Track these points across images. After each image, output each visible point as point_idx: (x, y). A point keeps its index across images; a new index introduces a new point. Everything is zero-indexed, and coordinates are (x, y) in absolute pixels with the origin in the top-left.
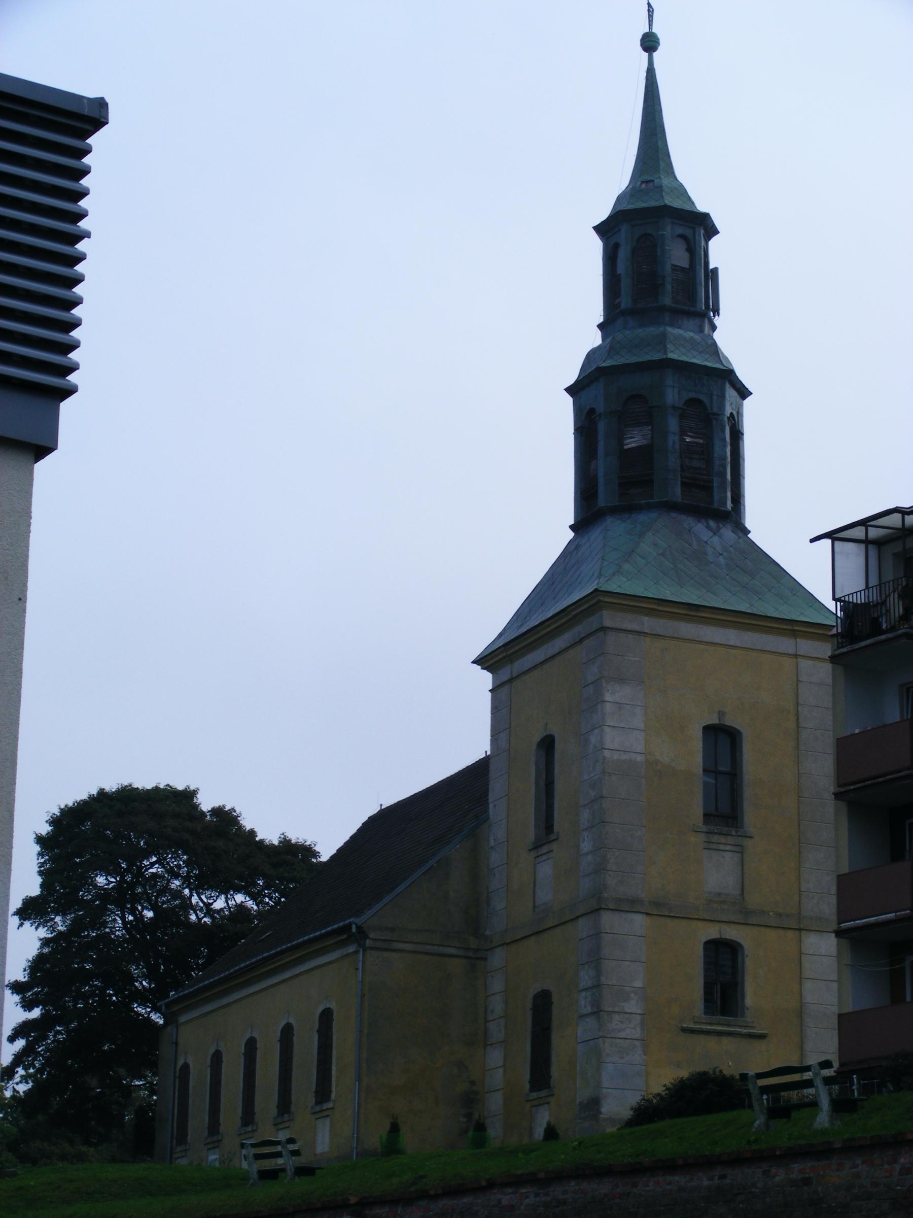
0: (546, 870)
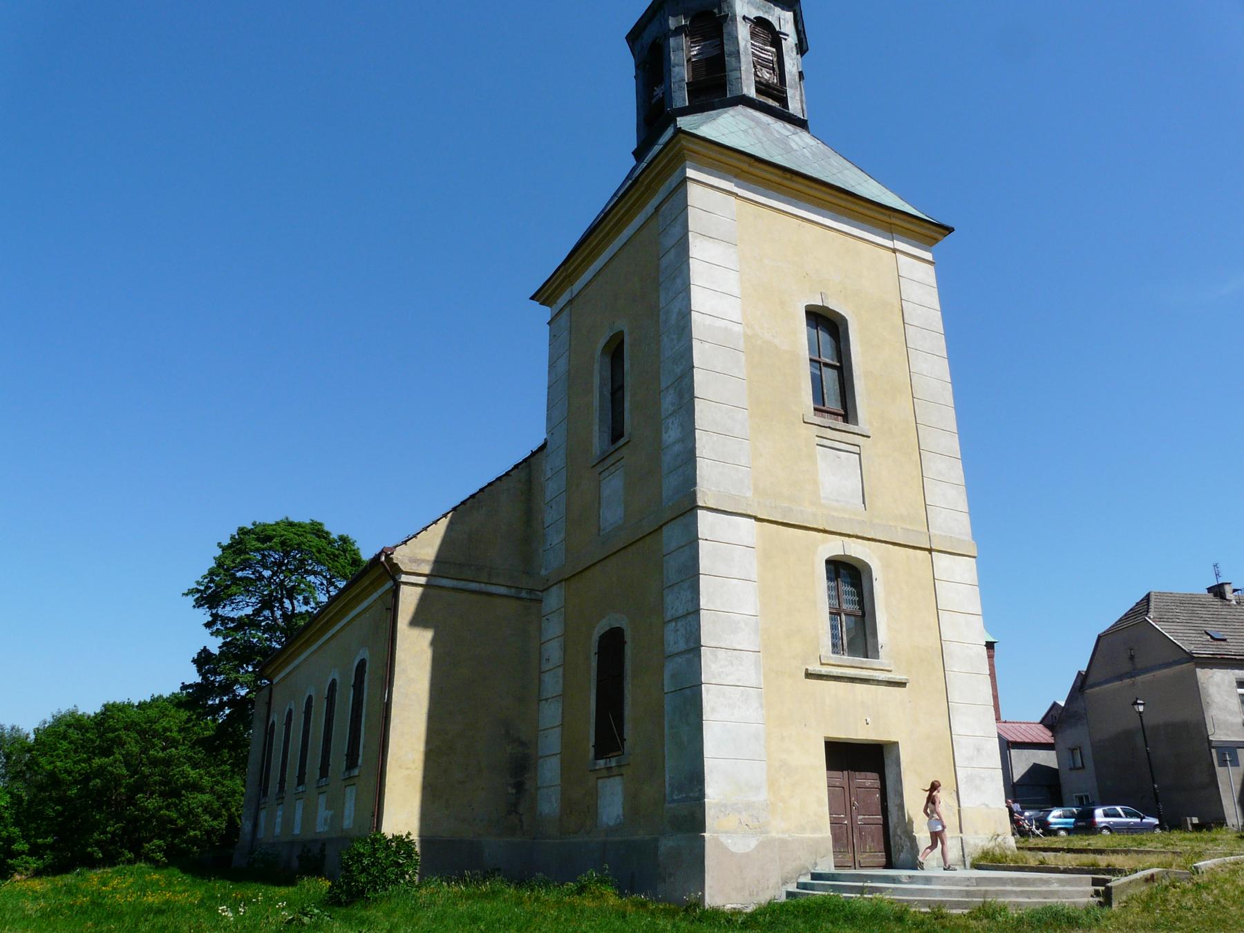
0: (613, 485)
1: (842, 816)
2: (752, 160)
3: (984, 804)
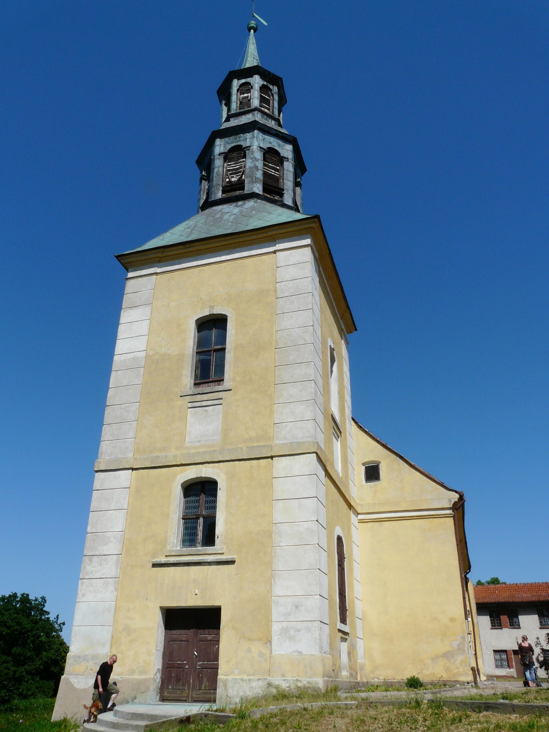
1: (185, 662)
2: (162, 250)
3: (297, 651)
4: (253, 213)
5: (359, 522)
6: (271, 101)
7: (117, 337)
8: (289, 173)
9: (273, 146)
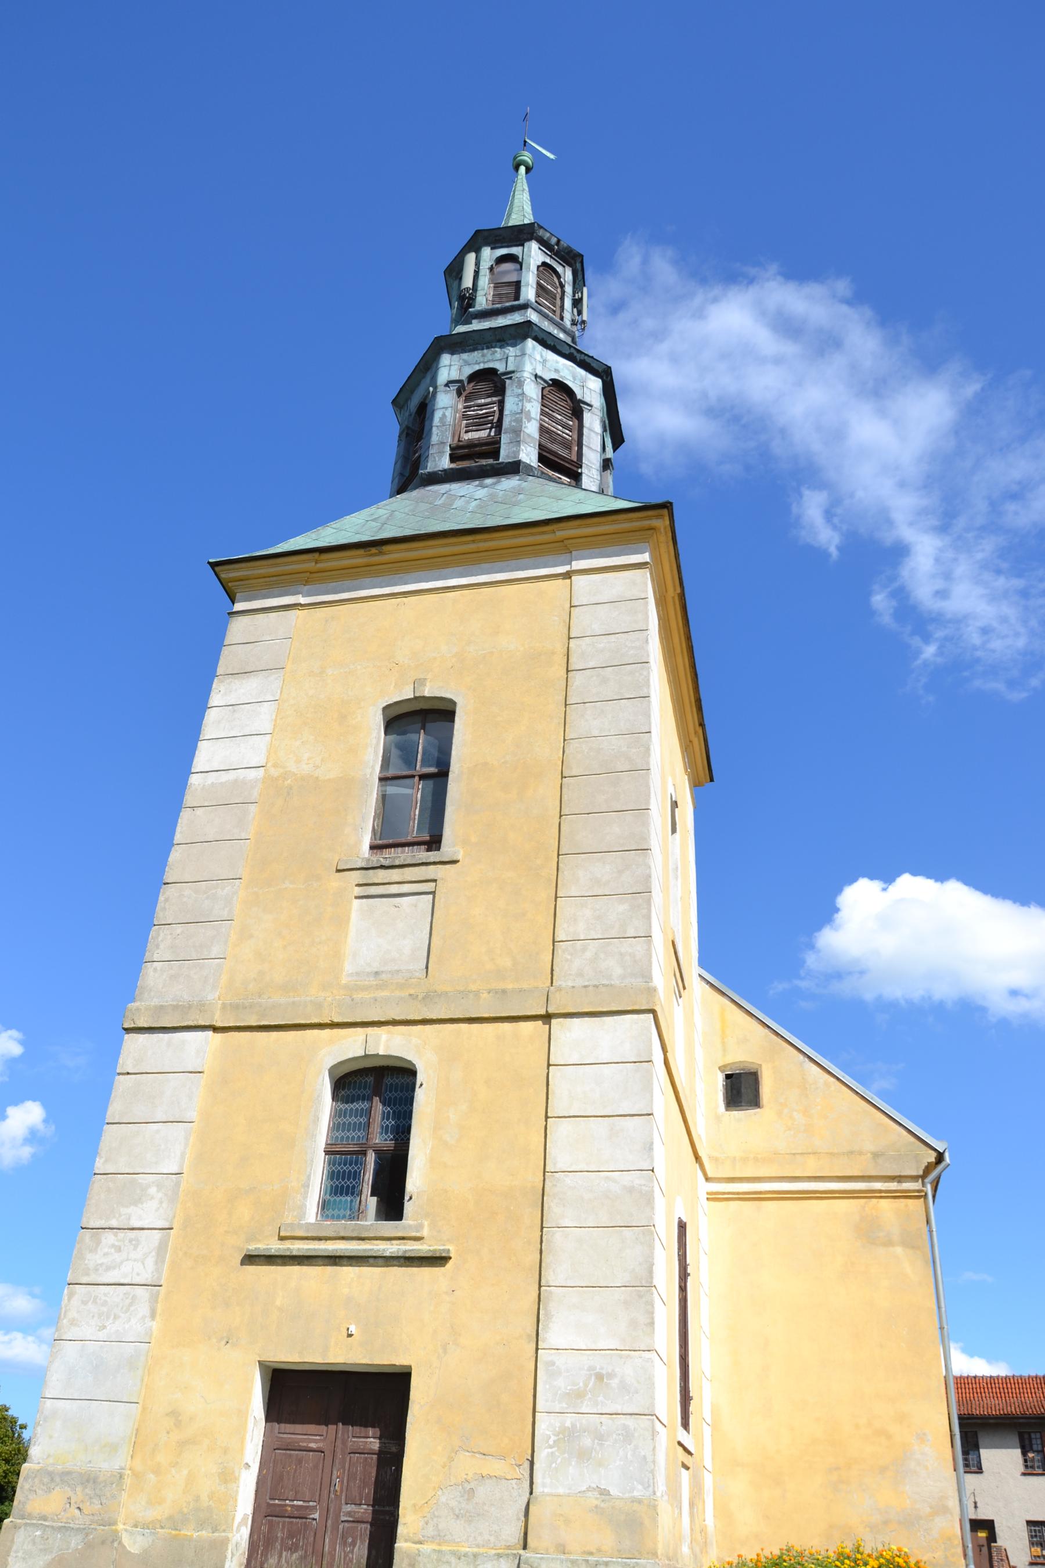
2: (316, 555)
4: (519, 499)
5: (707, 1199)
6: (558, 295)
7: (200, 733)
8: (593, 434)
9: (561, 377)
